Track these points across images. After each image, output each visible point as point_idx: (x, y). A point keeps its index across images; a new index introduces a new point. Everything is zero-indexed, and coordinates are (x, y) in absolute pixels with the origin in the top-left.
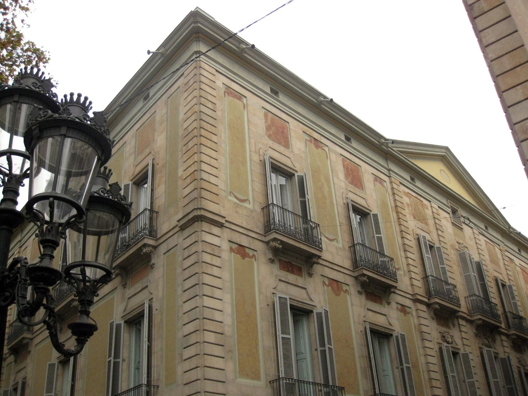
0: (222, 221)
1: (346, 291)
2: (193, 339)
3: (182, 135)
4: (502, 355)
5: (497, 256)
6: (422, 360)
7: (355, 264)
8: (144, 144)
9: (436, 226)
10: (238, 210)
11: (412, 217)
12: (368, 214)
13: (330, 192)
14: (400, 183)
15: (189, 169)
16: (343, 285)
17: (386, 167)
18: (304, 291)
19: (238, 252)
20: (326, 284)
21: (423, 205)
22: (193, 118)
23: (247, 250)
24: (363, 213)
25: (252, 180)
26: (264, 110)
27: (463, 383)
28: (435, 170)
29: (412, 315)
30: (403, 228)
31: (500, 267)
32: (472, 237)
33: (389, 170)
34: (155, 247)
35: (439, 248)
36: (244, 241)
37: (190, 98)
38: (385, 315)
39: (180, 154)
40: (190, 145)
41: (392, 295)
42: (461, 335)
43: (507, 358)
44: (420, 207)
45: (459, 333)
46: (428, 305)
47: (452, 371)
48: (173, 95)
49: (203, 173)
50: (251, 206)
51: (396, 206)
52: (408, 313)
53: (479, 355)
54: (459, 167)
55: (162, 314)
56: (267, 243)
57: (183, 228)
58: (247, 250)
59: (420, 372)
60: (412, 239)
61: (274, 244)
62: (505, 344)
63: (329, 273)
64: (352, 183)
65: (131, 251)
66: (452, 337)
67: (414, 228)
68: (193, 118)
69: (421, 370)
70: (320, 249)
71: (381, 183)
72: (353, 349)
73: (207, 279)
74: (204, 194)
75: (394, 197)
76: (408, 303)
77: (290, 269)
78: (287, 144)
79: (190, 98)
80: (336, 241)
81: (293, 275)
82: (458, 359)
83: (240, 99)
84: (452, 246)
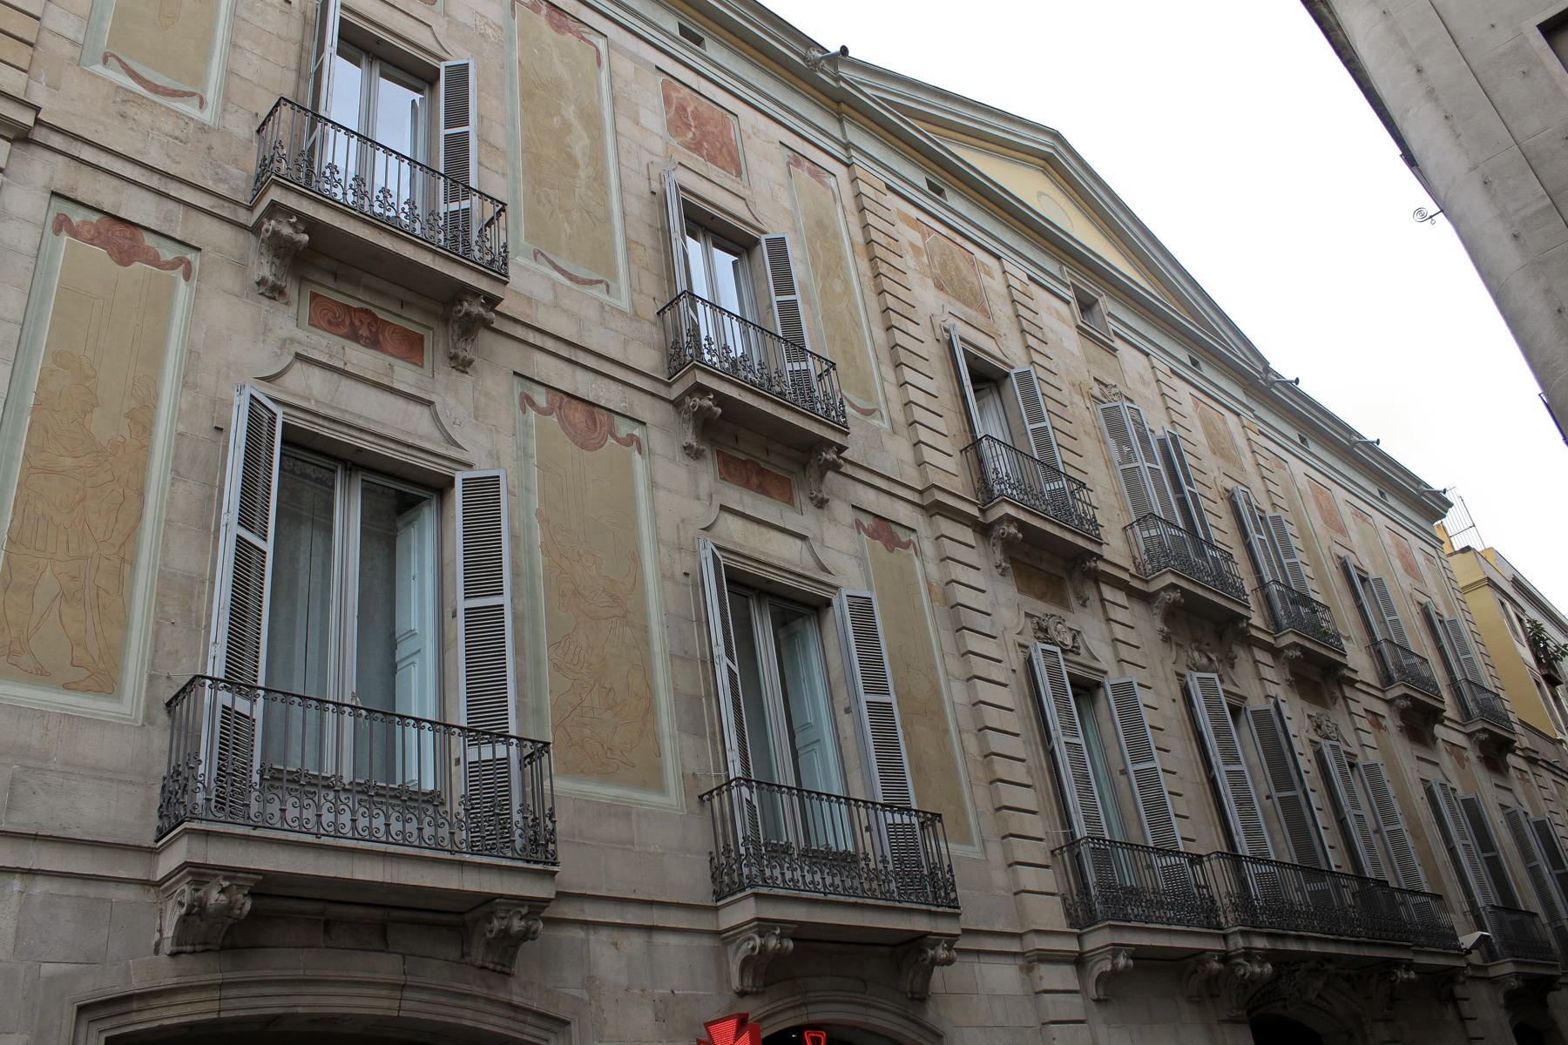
1: (631, 440)
4: (1256, 702)
5: (1232, 440)
6: (955, 694)
7: (1387, 680)
9: (1020, 323)
10: (131, 110)
11: (930, 282)
14: (888, 187)
16: (616, 418)
17: (838, 135)
18: (426, 411)
19: (873, 535)
20: (533, 404)
23: (149, 241)
24: (988, 378)
26: (661, 78)
27: (1123, 778)
29: (919, 552)
31: (1243, 469)
32: (1148, 376)
33: (847, 146)
35: (1025, 377)
38: (803, 538)
42: (1111, 631)
43: (1273, 710)
44: (963, 265)
45: (1104, 626)
46: (984, 530)
47: (1069, 728)
50: (207, 116)
51: (869, 242)
52: (906, 546)
53: (1178, 696)
54: (1122, 215)
56: (677, 404)
59: (946, 731)
60: (929, 339)
62: (1267, 673)
63: (869, 499)
66: (1076, 635)
67: (938, 312)
69: (952, 727)
72: (645, 629)
76: (902, 513)
77: (364, 332)
80: (603, 286)
81: (371, 352)
84: (1078, 387)
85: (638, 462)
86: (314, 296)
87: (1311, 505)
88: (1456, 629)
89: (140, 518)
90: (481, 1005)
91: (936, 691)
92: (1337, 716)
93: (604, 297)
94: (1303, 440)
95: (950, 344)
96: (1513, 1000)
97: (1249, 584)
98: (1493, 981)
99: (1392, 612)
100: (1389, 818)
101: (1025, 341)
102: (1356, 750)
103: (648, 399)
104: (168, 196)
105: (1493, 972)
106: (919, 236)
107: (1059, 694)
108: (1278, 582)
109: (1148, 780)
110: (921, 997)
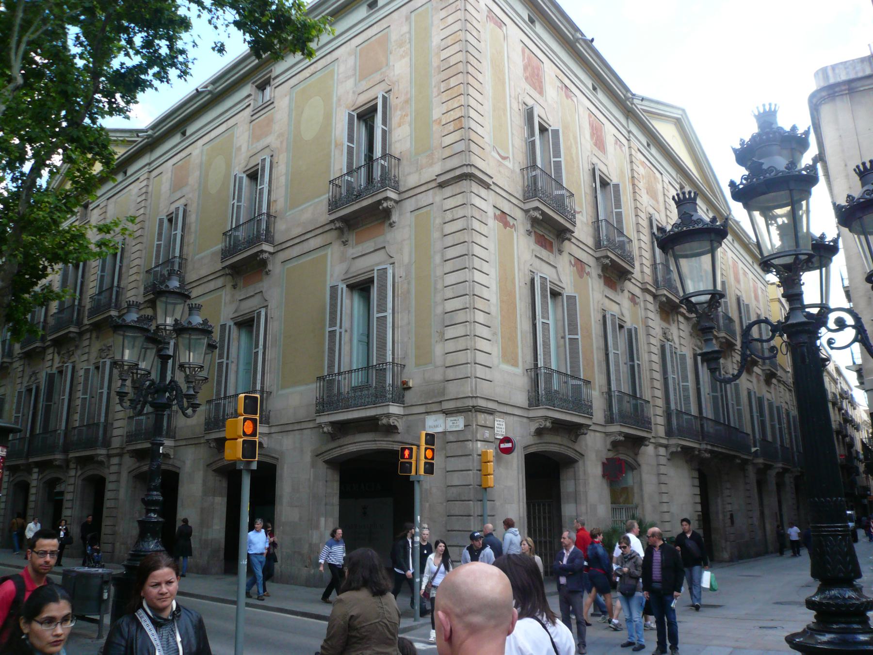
0: (489, 181)
1: (588, 274)
2: (461, 317)
3: (439, 67)
7: (598, 244)
8: (371, 64)
10: (501, 169)
12: (608, 184)
13: (577, 153)
15: (452, 112)
18: (554, 270)
21: (655, 178)
22: (457, 47)
23: (509, 218)
25: (512, 134)
28: (668, 133)
30: (638, 205)
33: (629, 132)
34: (397, 202)
36: (506, 207)
37: (450, 20)
39: (435, 92)
40: (453, 82)
41: (566, 242)
46: (655, 296)
48: (420, 10)
49: (471, 121)
51: (633, 177)
55: (409, 283)
56: (526, 211)
57: (442, 185)
58: (509, 218)
60: (644, 218)
61: (537, 214)
62: (682, 326)
64: (596, 145)
65: (365, 203)
68: (457, 47)
70: (574, 224)
71: (621, 147)
73: (477, 250)
74: (473, 147)
75: (632, 166)
78: (541, 92)
79: (450, 20)
83: (500, 27)
87: (732, 270)
94: (648, 145)
99: (557, 154)
102: (677, 346)
107: (544, 296)
110: (637, 454)
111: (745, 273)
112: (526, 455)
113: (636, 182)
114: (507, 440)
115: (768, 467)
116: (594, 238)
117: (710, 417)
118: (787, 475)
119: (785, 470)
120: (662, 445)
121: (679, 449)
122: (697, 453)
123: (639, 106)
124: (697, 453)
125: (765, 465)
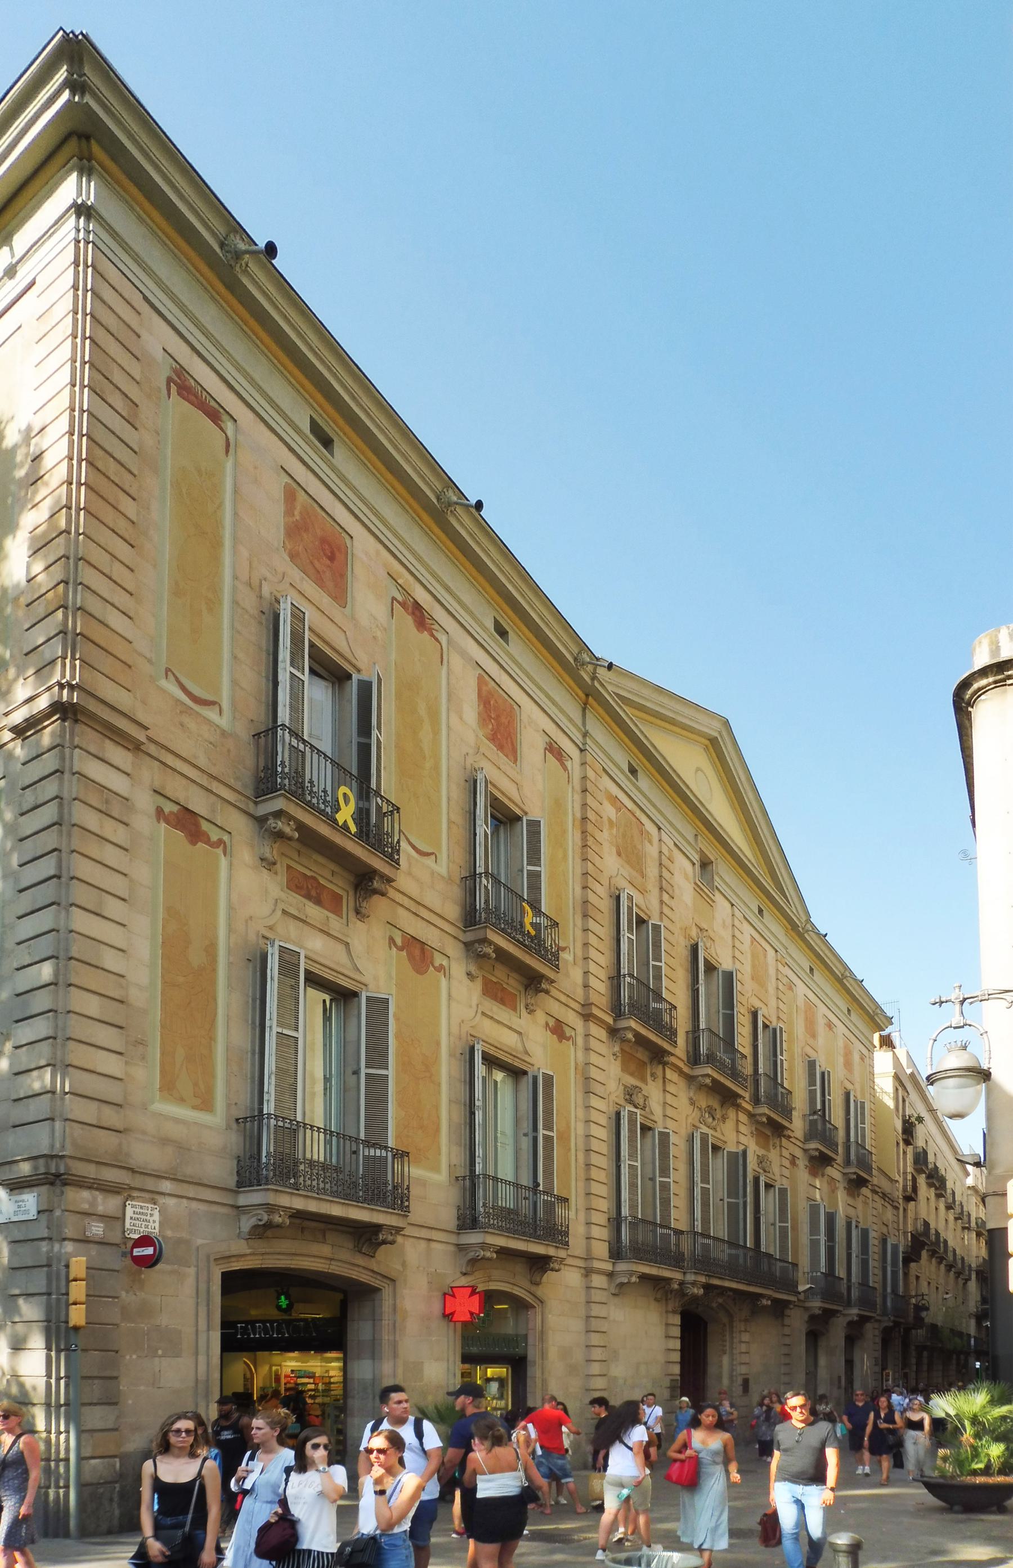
0: (141, 736)
1: (440, 968)
9: (661, 881)
10: (186, 720)
11: (614, 850)
28: (689, 762)
29: (575, 1044)
51: (584, 819)
52: (568, 1039)
59: (570, 1150)
62: (743, 1128)
64: (493, 738)
75: (584, 798)
80: (433, 857)
81: (317, 907)
82: (353, 1021)
85: (444, 982)
86: (289, 867)
88: (863, 1108)
89: (215, 1015)
90: (361, 1270)
91: (569, 1127)
92: (773, 1155)
93: (433, 865)
95: (618, 898)
96: (813, 1318)
97: (682, 1023)
98: (806, 1309)
100: (783, 1217)
101: (661, 896)
103: (202, 792)
104: (211, 792)
105: (807, 1304)
106: (614, 811)
108: (631, 975)
109: (665, 1187)
111: (830, 1025)
112: (223, 1273)
113: (590, 827)
114: (145, 1241)
115: (828, 1315)
116: (464, 907)
117: (720, 1235)
118: (869, 1326)
119: (863, 1319)
120: (600, 1272)
121: (634, 1279)
122: (676, 1286)
123: (609, 684)
124: (676, 1286)
125: (825, 1310)
